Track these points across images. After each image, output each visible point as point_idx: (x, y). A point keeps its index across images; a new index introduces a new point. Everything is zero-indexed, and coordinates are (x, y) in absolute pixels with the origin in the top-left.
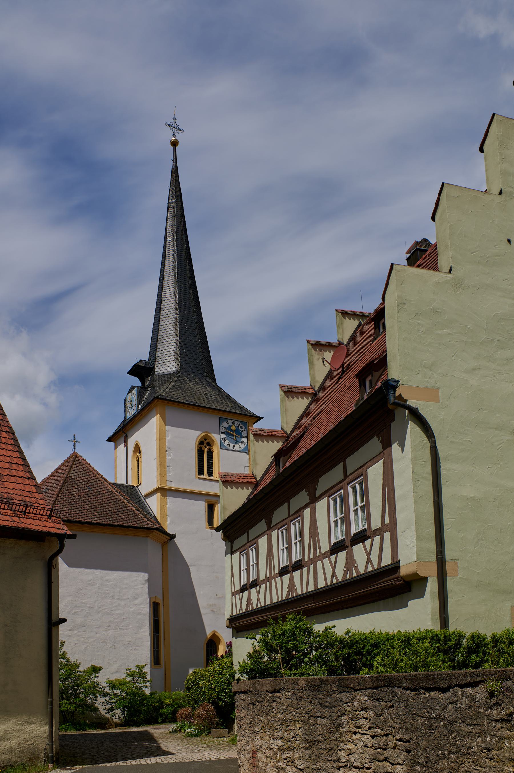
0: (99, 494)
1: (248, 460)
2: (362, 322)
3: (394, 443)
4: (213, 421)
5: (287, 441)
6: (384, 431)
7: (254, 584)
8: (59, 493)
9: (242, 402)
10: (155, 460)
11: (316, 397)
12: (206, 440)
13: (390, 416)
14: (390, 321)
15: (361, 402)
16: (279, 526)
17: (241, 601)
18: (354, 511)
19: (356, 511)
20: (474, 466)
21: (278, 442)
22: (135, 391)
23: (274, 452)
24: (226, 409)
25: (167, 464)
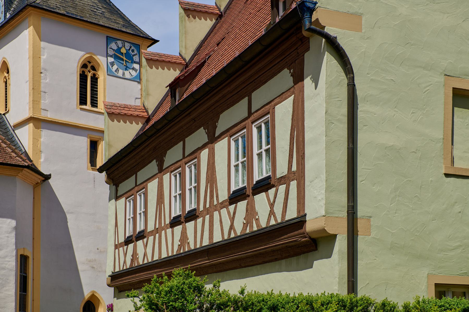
1: (140, 90)
3: (307, 77)
5: (185, 69)
6: (296, 61)
7: (141, 236)
9: (135, 21)
12: (90, 62)
13: (304, 44)
17: (125, 255)
19: (260, 155)
20: (396, 110)
23: (170, 82)
24: (116, 26)
25: (43, 89)
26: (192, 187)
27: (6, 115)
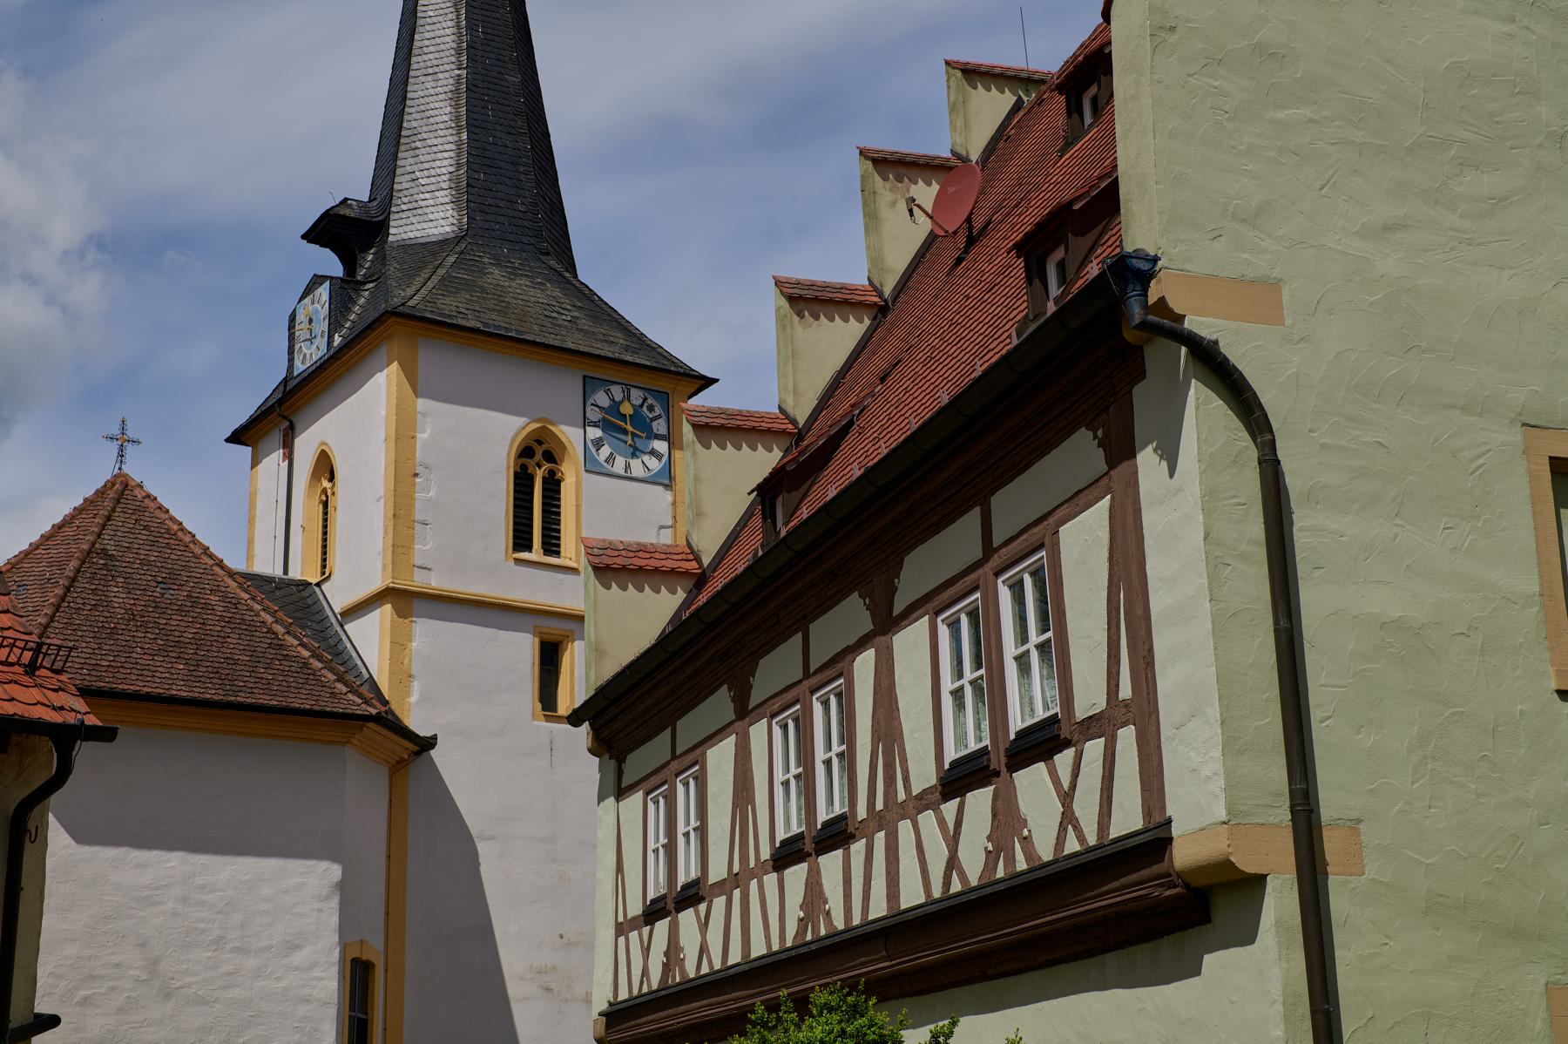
0: (195, 604)
1: (705, 501)
2: (1025, 99)
3: (1144, 447)
4: (564, 388)
7: (691, 896)
8: (63, 600)
10: (384, 503)
11: (885, 316)
12: (540, 442)
13: (1131, 366)
14: (1128, 82)
15: (1032, 327)
16: (772, 708)
17: (646, 951)
18: (1016, 659)
19: (1022, 661)
21: (770, 450)
22: (323, 292)
24: (606, 351)
25: (418, 516)
26: (832, 754)
27: (323, 587)
